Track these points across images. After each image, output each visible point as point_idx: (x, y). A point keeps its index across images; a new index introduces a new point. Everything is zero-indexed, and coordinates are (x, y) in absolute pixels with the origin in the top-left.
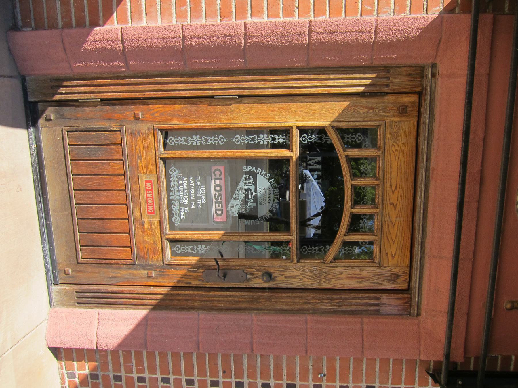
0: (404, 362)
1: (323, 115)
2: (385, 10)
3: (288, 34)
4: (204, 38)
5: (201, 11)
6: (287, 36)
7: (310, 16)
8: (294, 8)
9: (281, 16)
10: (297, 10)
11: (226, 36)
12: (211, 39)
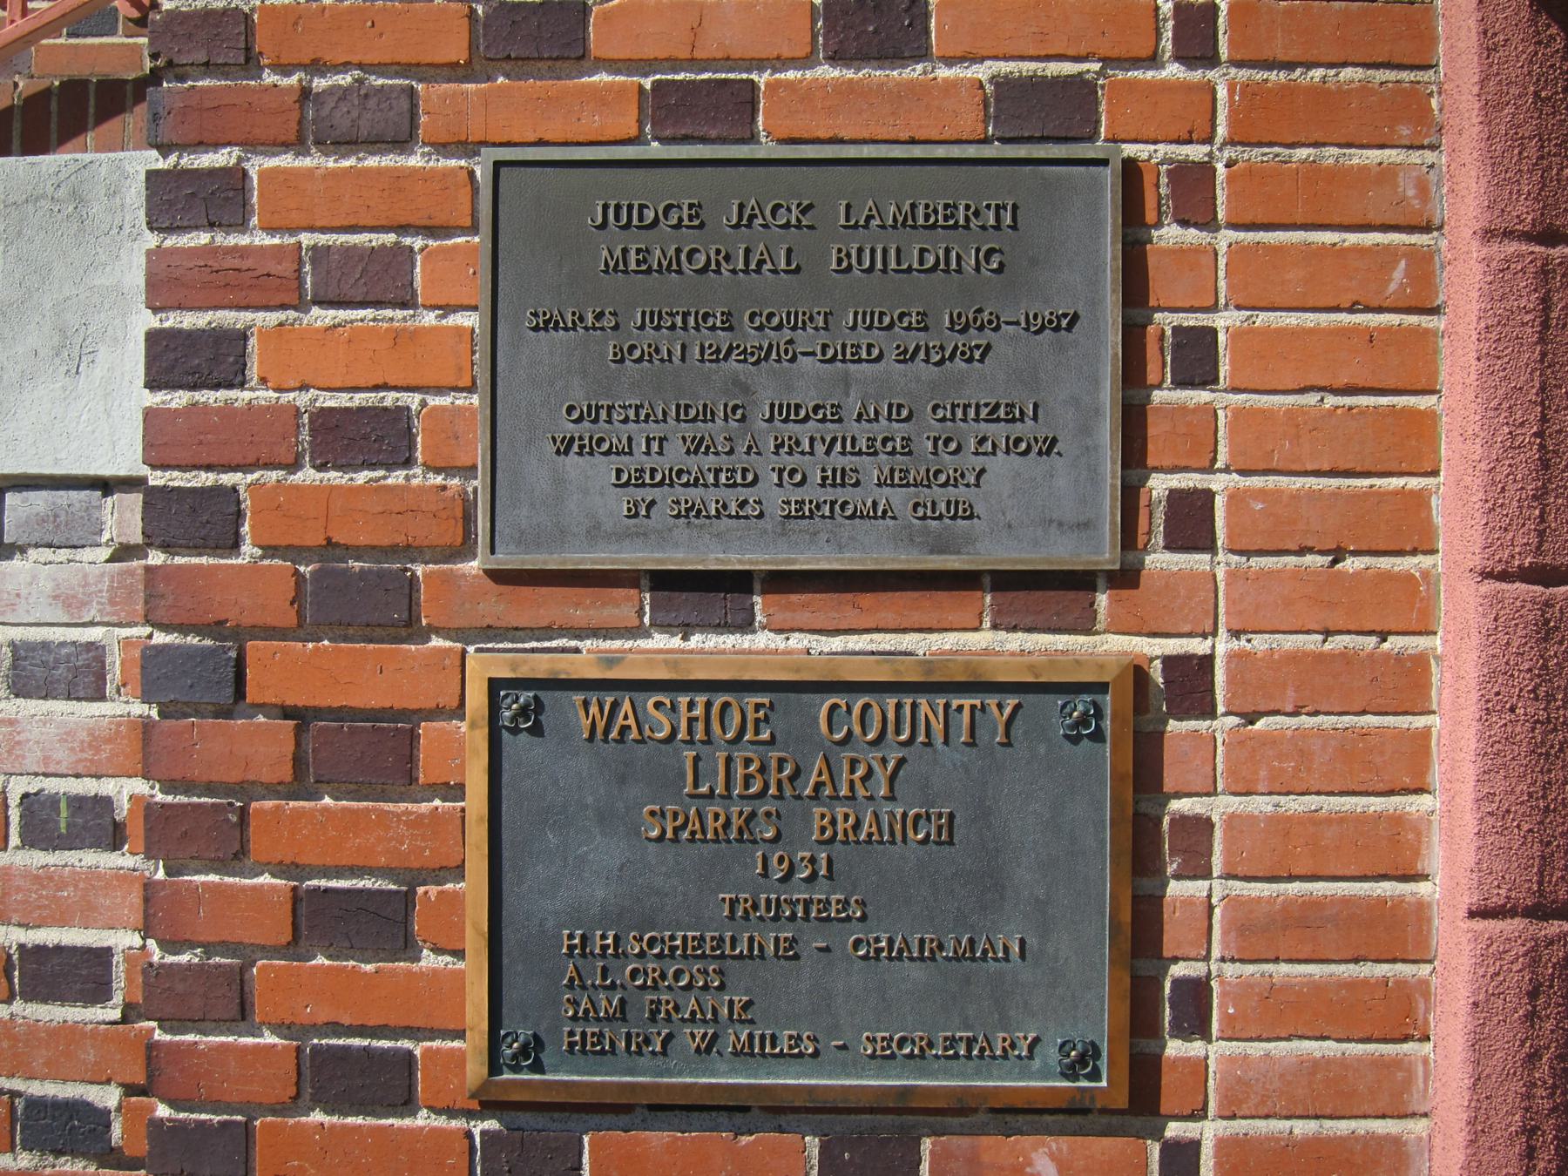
0: (1197, 75)
2: (1411, 193)
3: (1541, 692)
4: (1534, 1129)
5: (1371, 1137)
6: (1550, 698)
7: (1426, 574)
8: (1387, 655)
9: (1420, 722)
10: (1394, 643)
11: (1531, 1016)
12: (1541, 1092)
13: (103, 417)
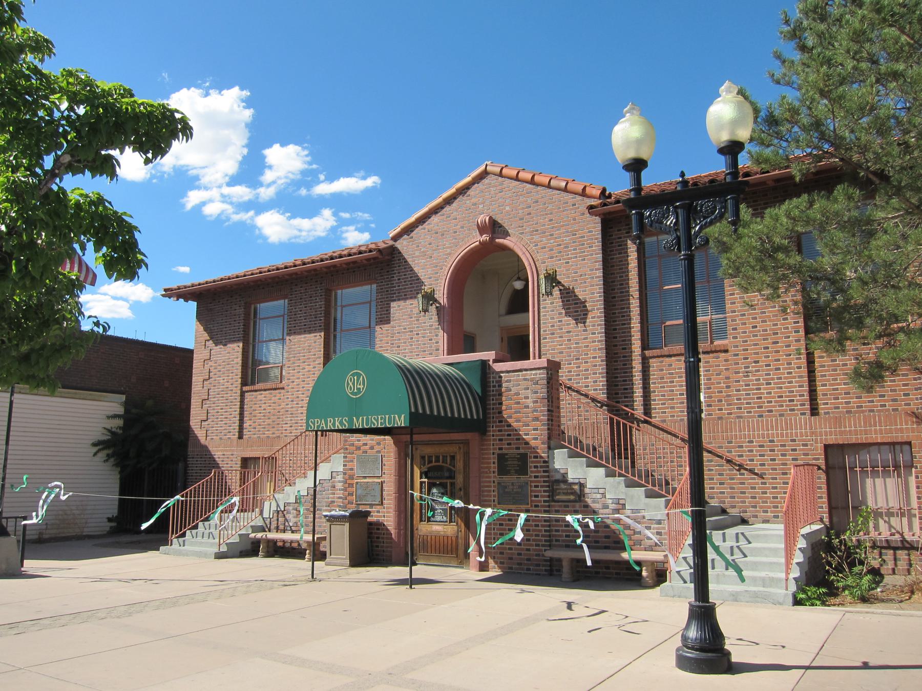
1: (417, 472)
13: (341, 469)
